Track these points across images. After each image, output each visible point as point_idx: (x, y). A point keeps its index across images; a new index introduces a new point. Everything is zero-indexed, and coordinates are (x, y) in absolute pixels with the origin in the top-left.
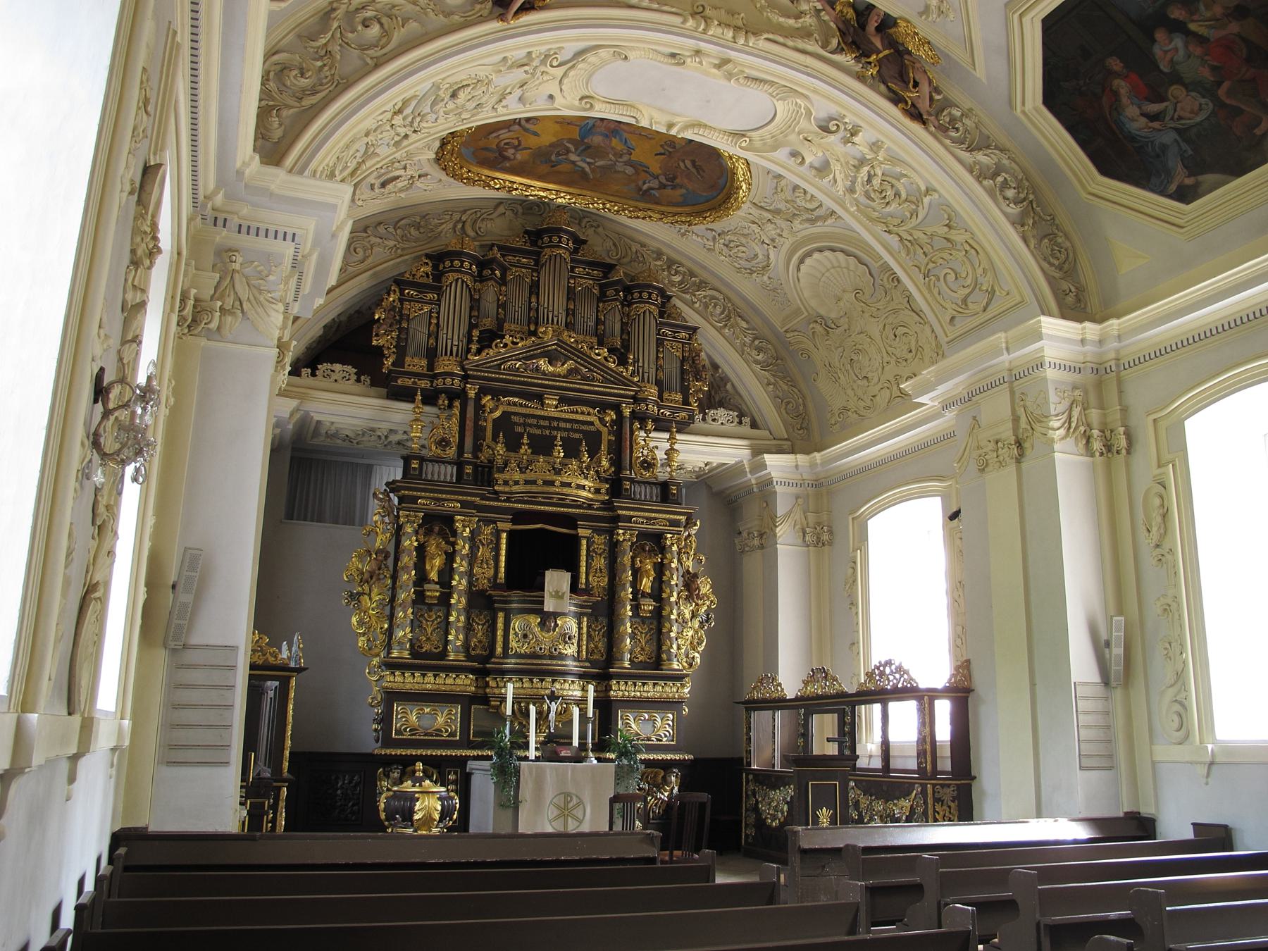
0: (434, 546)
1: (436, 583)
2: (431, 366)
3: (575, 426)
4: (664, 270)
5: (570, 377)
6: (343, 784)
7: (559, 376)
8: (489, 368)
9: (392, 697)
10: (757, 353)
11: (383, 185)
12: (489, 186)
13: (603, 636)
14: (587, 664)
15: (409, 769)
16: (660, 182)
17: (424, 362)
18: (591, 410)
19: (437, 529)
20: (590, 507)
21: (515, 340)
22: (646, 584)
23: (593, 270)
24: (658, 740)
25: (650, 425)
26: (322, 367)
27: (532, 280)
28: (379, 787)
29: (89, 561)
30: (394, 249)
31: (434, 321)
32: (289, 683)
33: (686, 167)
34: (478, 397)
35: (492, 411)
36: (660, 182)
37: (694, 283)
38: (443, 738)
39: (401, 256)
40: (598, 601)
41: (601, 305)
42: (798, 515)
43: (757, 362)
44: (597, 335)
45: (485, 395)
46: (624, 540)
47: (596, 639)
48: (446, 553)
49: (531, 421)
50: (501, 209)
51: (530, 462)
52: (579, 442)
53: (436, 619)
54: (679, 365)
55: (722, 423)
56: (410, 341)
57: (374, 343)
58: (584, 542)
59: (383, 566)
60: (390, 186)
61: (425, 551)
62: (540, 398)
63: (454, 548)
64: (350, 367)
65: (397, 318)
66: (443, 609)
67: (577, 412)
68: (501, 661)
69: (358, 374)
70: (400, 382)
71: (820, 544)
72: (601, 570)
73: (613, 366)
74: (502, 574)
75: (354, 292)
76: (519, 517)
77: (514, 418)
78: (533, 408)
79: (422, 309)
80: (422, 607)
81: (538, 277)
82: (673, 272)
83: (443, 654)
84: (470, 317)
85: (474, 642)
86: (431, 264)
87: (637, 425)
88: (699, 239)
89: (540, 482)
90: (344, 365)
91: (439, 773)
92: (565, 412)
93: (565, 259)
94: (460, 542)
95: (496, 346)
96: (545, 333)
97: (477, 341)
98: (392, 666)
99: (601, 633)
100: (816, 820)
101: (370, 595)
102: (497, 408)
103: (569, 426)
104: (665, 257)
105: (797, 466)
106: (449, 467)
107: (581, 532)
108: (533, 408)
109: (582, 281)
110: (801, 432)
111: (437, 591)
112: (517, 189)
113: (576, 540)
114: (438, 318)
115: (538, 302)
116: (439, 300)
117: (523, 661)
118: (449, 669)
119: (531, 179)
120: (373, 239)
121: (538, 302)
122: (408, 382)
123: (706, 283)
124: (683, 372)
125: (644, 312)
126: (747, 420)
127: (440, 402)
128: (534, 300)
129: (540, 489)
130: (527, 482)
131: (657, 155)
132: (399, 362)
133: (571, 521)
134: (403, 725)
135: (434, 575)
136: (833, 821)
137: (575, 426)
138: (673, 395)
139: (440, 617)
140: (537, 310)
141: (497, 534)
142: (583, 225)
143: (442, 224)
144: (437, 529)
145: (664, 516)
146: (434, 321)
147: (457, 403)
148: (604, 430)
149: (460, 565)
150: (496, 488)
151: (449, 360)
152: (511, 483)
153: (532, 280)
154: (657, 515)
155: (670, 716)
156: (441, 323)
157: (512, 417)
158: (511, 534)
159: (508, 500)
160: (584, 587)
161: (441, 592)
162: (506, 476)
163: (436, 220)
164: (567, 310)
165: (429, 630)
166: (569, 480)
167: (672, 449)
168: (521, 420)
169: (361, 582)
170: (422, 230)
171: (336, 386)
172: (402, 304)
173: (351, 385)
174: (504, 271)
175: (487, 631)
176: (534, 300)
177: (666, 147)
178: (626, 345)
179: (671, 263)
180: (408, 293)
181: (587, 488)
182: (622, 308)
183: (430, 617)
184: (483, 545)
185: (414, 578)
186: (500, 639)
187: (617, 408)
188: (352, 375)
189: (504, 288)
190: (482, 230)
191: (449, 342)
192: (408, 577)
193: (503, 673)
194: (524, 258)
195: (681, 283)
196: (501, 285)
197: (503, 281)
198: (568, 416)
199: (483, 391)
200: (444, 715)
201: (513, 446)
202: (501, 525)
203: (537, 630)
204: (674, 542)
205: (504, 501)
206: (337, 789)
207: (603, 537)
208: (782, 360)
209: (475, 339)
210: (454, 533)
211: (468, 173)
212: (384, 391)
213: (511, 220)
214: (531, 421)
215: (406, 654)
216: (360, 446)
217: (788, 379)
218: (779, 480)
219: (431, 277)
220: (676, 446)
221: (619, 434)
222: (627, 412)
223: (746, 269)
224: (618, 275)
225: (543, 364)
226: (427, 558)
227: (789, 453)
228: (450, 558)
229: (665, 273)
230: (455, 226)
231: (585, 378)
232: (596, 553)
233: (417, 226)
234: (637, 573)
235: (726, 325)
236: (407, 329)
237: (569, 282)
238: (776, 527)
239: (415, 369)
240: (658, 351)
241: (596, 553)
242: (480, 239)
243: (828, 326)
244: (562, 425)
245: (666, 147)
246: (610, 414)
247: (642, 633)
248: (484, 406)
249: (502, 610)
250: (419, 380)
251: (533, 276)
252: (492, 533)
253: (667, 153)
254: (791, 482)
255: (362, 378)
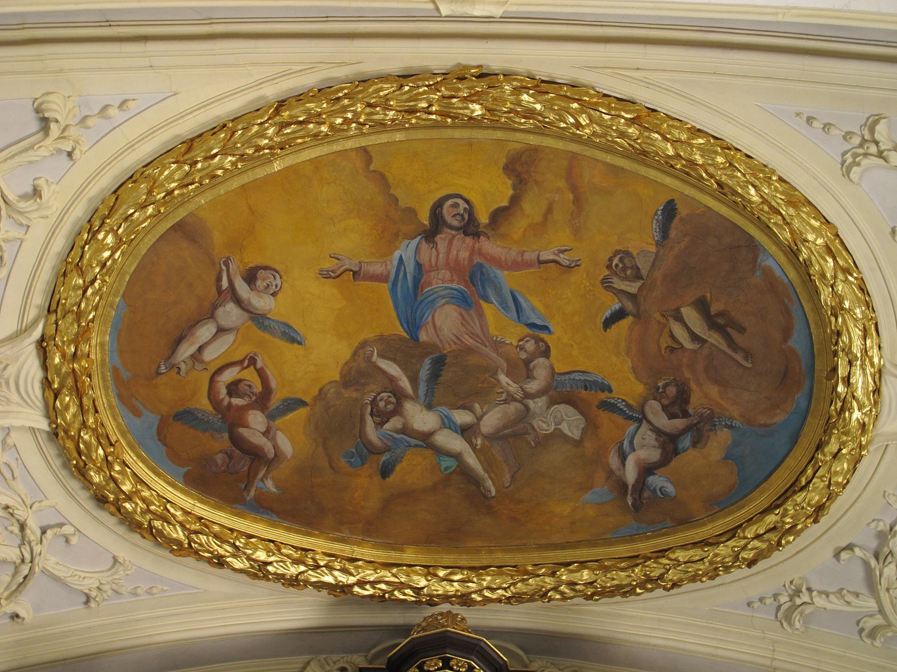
16: (658, 431)
29: (881, 114)
33: (695, 337)
36: (658, 431)
88: (835, 604)
131: (608, 323)
177: (618, 284)
245: (618, 284)
253: (629, 306)
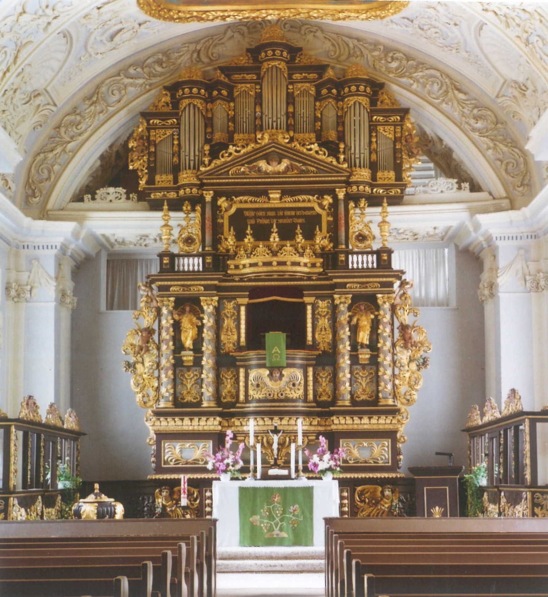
0: (186, 322)
1: (190, 350)
2: (176, 181)
3: (298, 213)
4: (381, 59)
5: (288, 173)
6: (148, 503)
7: (279, 173)
8: (220, 175)
9: (162, 436)
10: (475, 121)
11: (112, 38)
12: (202, 19)
13: (329, 382)
14: (314, 404)
15: (176, 489)
17: (171, 177)
18: (311, 197)
19: (188, 309)
20: (309, 279)
21: (238, 149)
22: (364, 337)
23: (309, 74)
24: (375, 462)
25: (363, 202)
26: (101, 192)
27: (256, 92)
28: (157, 503)
30: (144, 85)
31: (176, 142)
32: (10, 429)
34: (214, 200)
35: (226, 210)
37: (412, 66)
38: (200, 466)
39: (149, 91)
40: (320, 354)
41: (318, 104)
42: (519, 265)
43: (474, 130)
44: (315, 132)
45: (220, 197)
46: (341, 303)
47: (324, 384)
48: (197, 326)
49: (261, 214)
50: (230, 33)
51: (255, 248)
52: (294, 226)
53: (193, 377)
54: (392, 146)
55: (442, 192)
56: (158, 164)
57: (131, 167)
58: (309, 308)
59: (151, 340)
60: (117, 39)
61: (181, 326)
62: (265, 193)
63: (202, 322)
64: (121, 188)
65: (146, 144)
66: (374, 368)
67: (299, 201)
68: (243, 405)
69: (128, 194)
70: (152, 196)
71: (540, 289)
72: (325, 329)
73: (324, 157)
74: (243, 339)
75: (116, 127)
76: (254, 292)
77: (247, 213)
78: (260, 203)
79: (166, 134)
80: (182, 368)
81: (261, 88)
82: (389, 60)
83: (199, 404)
84: (206, 134)
85: (224, 392)
86: (169, 94)
87: (352, 204)
88: (399, 27)
89: (275, 263)
90: (115, 187)
91: (199, 491)
92: (289, 202)
93: (281, 69)
94: (206, 317)
95: (223, 157)
96: (262, 138)
97: (209, 154)
98: (159, 414)
99: (328, 379)
100: (430, 514)
101: (143, 363)
102: (231, 206)
103: (293, 213)
104: (382, 48)
105: (511, 222)
106: (196, 259)
107: (307, 300)
108: (260, 203)
109: (299, 85)
110: (521, 189)
111: (191, 356)
112: (229, 16)
113: (303, 306)
114: (179, 139)
115: (262, 113)
116: (179, 124)
117: (261, 404)
118: (201, 414)
119: (239, 5)
120: (127, 81)
121: (262, 113)
122: (159, 195)
123: (423, 64)
124: (395, 151)
125: (355, 103)
126: (466, 185)
127: (184, 208)
128: (258, 109)
129: (275, 269)
130: (251, 265)
132: (151, 181)
133: (298, 292)
134: (170, 457)
135: (188, 343)
136: (444, 514)
137: (298, 213)
138: (386, 173)
139: (372, 373)
140: (261, 118)
141: (238, 307)
142: (303, 32)
143: (181, 56)
144: (188, 309)
145: (375, 280)
146: (176, 142)
147: (198, 208)
148: (324, 213)
149: (207, 335)
150: (229, 272)
151: (187, 173)
152: (241, 267)
153: (256, 92)
154: (368, 280)
155: (386, 443)
156: (182, 143)
157: (245, 212)
158: (249, 307)
159: (241, 280)
160: (310, 343)
161: (371, 355)
162: (236, 262)
163: (175, 54)
164: (287, 113)
165: (189, 386)
166: (284, 259)
167: (384, 222)
168: (252, 214)
169: (135, 354)
170: (164, 65)
171: (111, 205)
172: (149, 132)
173: (123, 203)
174: (230, 89)
175: (234, 383)
176: (258, 109)
178: (341, 137)
179: (387, 50)
180: (153, 122)
181: (302, 264)
182: (337, 103)
183: (189, 376)
184: (227, 317)
185: (172, 348)
186: (242, 389)
187: (332, 193)
188: (123, 195)
189: (232, 104)
190: (214, 55)
191: (187, 158)
192: (167, 348)
193: (245, 415)
194: (248, 74)
195: (397, 69)
196: (229, 102)
197: (231, 98)
198: (291, 205)
199: (217, 195)
200: (200, 448)
201: (240, 236)
202: (240, 301)
203: (267, 380)
204: (386, 300)
205: (239, 281)
206: (144, 507)
207: (326, 302)
208: (502, 123)
209: (207, 152)
210: (203, 312)
211: (177, 14)
212: (145, 204)
213: (239, 41)
214: (261, 214)
215: (170, 405)
216: (147, 248)
217: (509, 140)
218: (498, 236)
219: (170, 105)
220: (387, 219)
221: (335, 215)
222: (341, 195)
223: (446, 47)
224: (330, 73)
225: (263, 164)
226: (182, 332)
227: (507, 210)
228: (200, 329)
229: (383, 62)
230: (192, 56)
231: (302, 172)
232: (321, 315)
233: (160, 63)
234: (355, 330)
235: (443, 100)
236: (155, 153)
237: (288, 89)
238: (497, 277)
239: (163, 185)
240: (370, 136)
241: (321, 315)
242: (215, 63)
243: (522, 88)
244: (288, 213)
246: (327, 199)
247: (362, 377)
248: (220, 206)
249: (242, 366)
250: (168, 192)
251: (256, 89)
252: (234, 307)
254: (511, 236)
255: (131, 196)
